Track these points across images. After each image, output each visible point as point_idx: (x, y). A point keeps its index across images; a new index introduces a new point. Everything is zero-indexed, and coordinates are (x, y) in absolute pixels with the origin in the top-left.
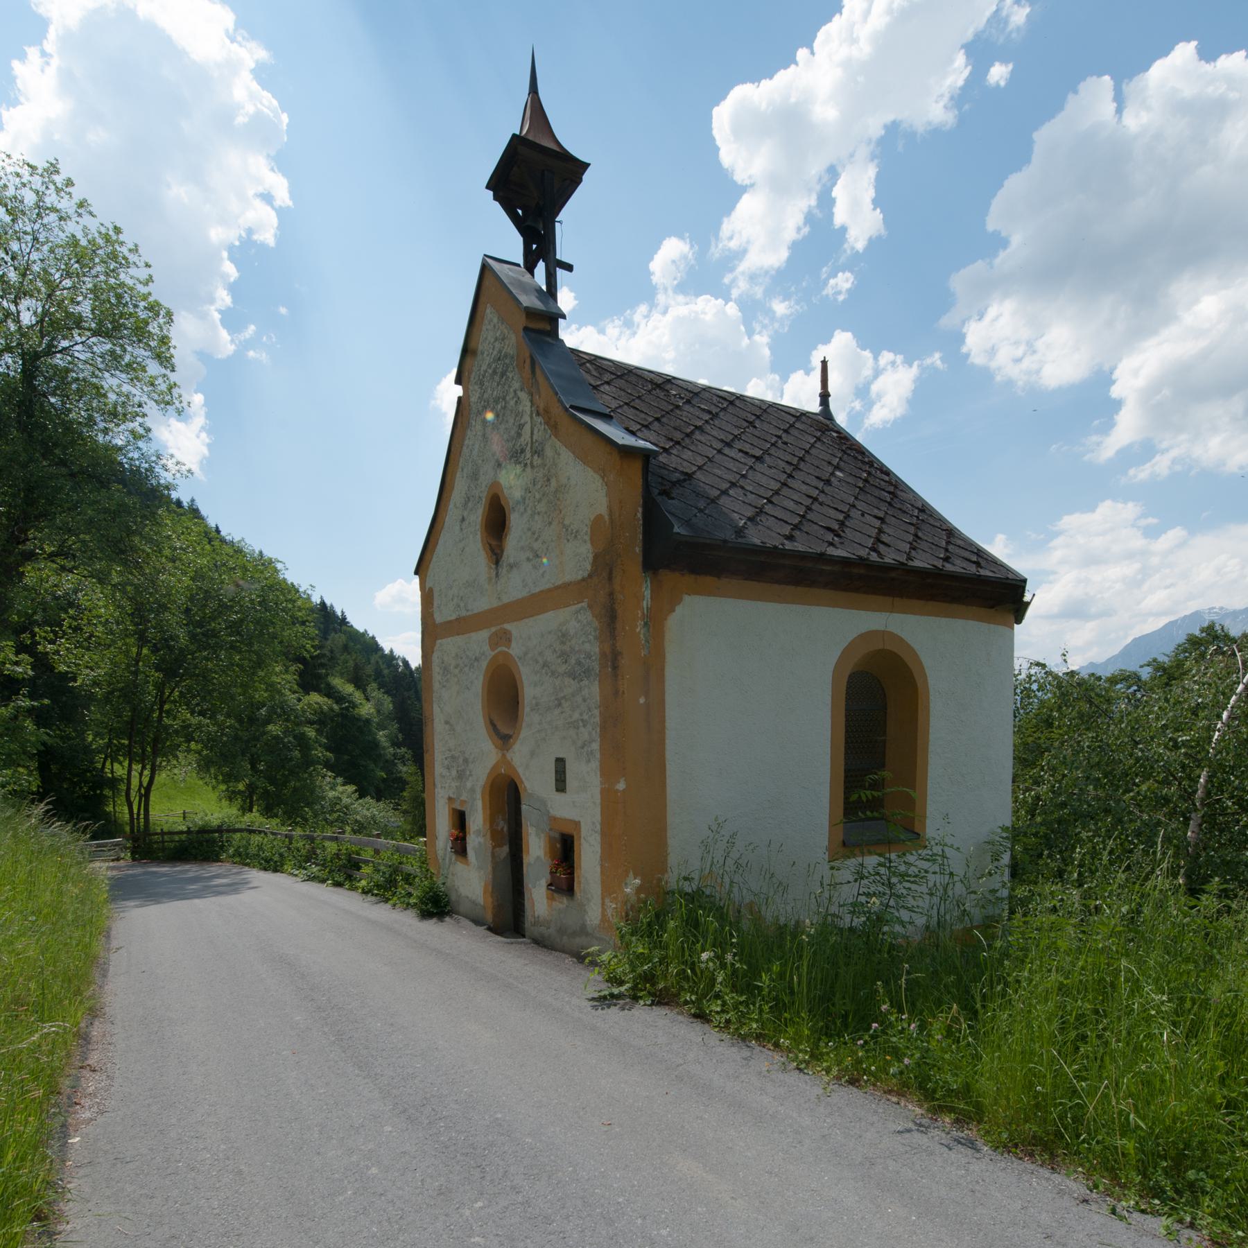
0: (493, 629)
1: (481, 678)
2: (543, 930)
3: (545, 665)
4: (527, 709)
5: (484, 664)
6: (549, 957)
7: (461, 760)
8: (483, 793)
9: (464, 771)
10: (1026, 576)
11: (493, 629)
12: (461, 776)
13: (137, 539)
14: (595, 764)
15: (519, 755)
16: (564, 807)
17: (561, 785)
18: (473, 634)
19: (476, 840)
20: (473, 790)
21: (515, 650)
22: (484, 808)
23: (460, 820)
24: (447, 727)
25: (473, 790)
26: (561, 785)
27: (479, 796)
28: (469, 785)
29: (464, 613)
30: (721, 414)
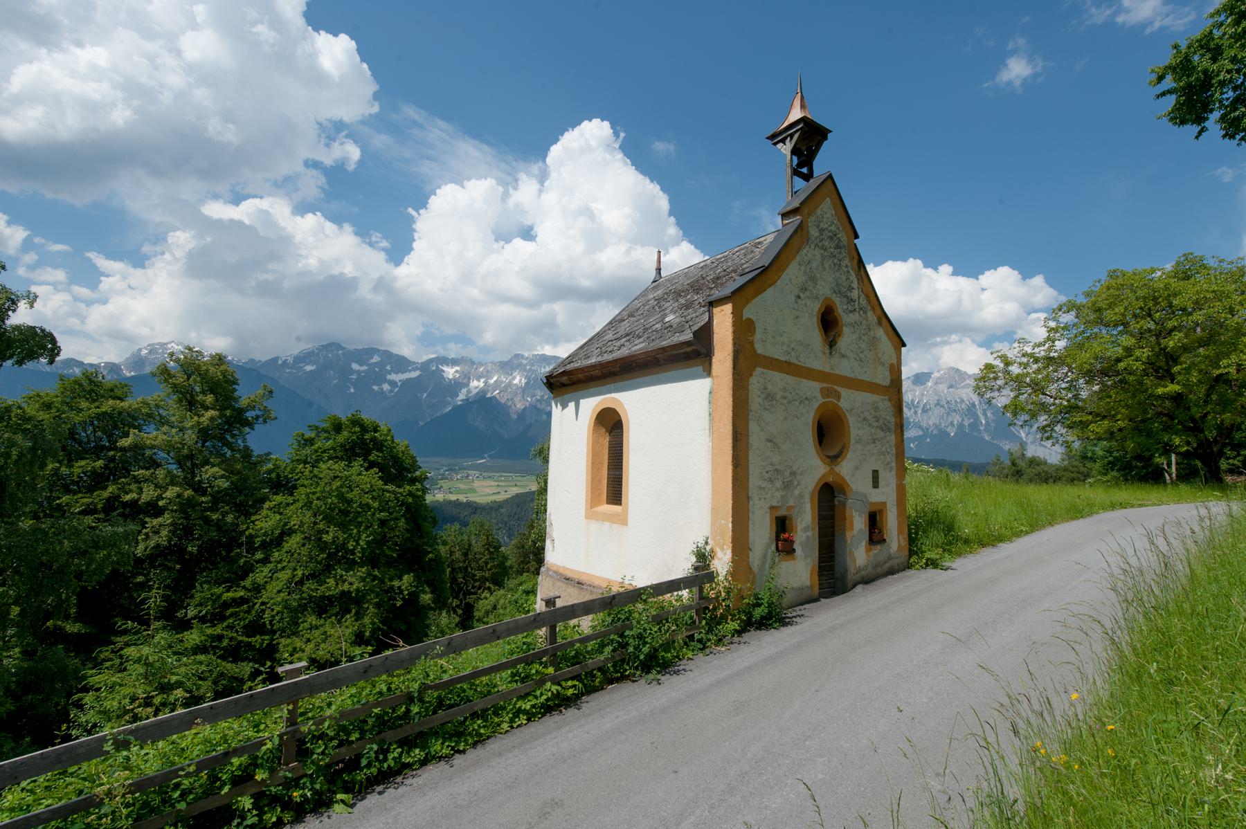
0: (825, 385)
1: (812, 414)
2: (864, 573)
3: (865, 419)
4: (852, 442)
5: (816, 405)
6: (878, 583)
7: (787, 473)
8: (812, 497)
9: (791, 481)
10: (594, 526)
11: (825, 385)
12: (787, 486)
13: (1013, 791)
14: (894, 472)
15: (845, 468)
16: (876, 496)
17: (876, 484)
18: (805, 381)
19: (858, 524)
20: (801, 496)
21: (844, 404)
22: (812, 509)
23: (782, 525)
24: (769, 445)
25: (801, 496)
26: (876, 484)
27: (807, 499)
28: (797, 492)
29: (794, 361)
30: (313, 519)
